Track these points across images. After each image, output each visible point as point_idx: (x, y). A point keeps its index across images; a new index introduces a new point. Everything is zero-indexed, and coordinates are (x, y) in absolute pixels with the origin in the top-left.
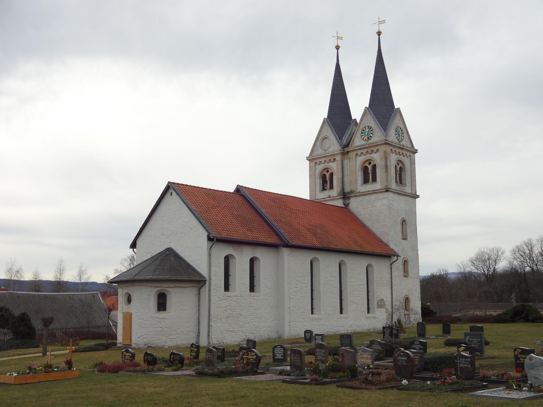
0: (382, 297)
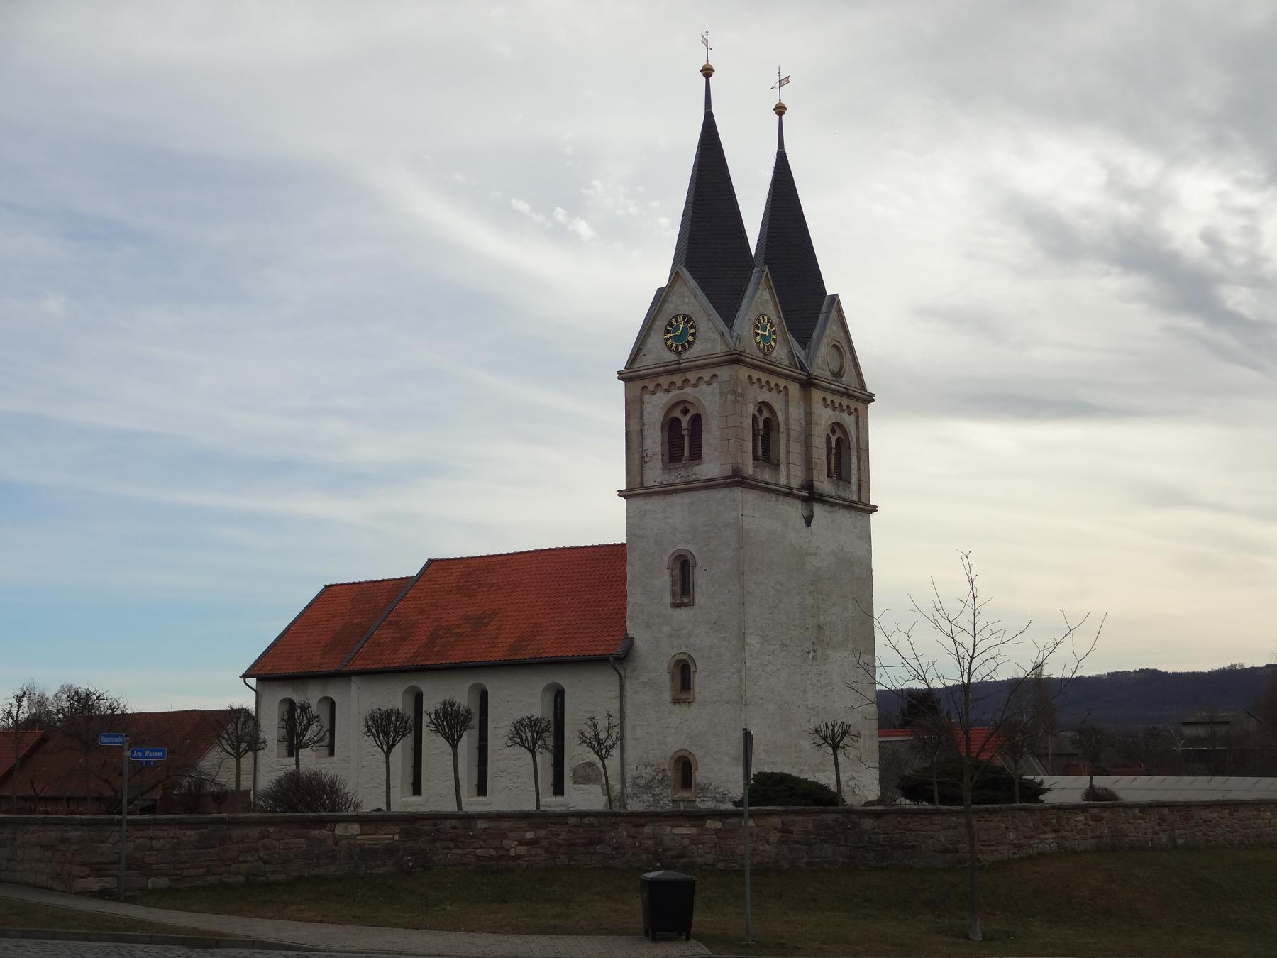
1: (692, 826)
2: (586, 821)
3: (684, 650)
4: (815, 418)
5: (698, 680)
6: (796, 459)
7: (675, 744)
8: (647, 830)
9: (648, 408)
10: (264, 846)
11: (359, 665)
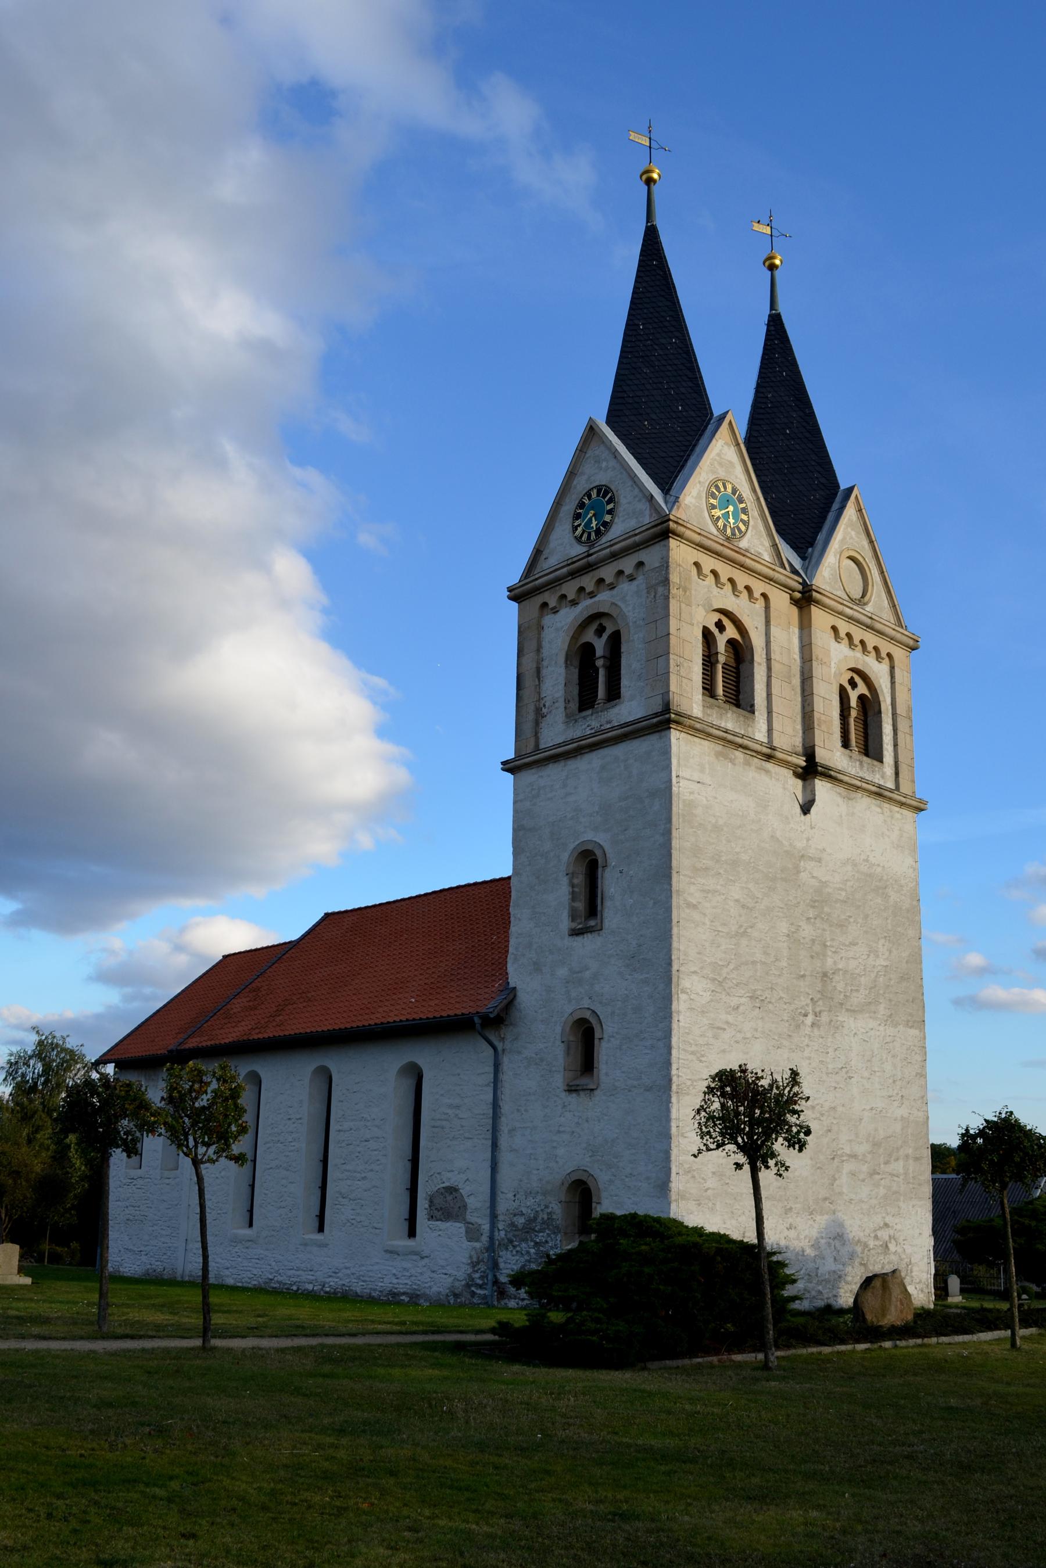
0: (453, 1179)
3: (586, 1003)
4: (817, 651)
5: (604, 1052)
7: (570, 1159)
9: (548, 635)
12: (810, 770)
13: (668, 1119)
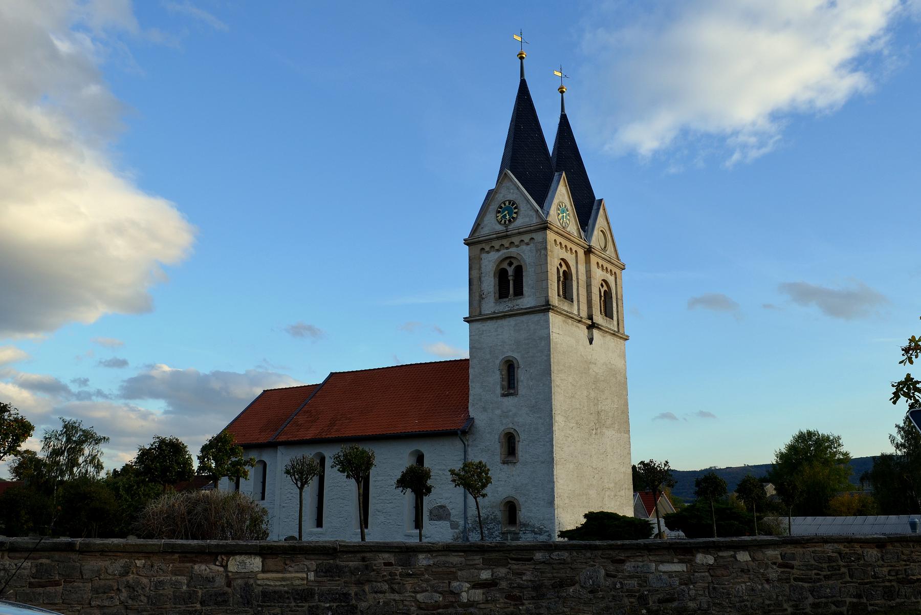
1: (681, 561)
2: (555, 555)
3: (511, 426)
4: (592, 273)
5: (520, 447)
6: (583, 299)
8: (629, 566)
10: (128, 586)
11: (283, 438)
12: (592, 326)
13: (553, 475)
